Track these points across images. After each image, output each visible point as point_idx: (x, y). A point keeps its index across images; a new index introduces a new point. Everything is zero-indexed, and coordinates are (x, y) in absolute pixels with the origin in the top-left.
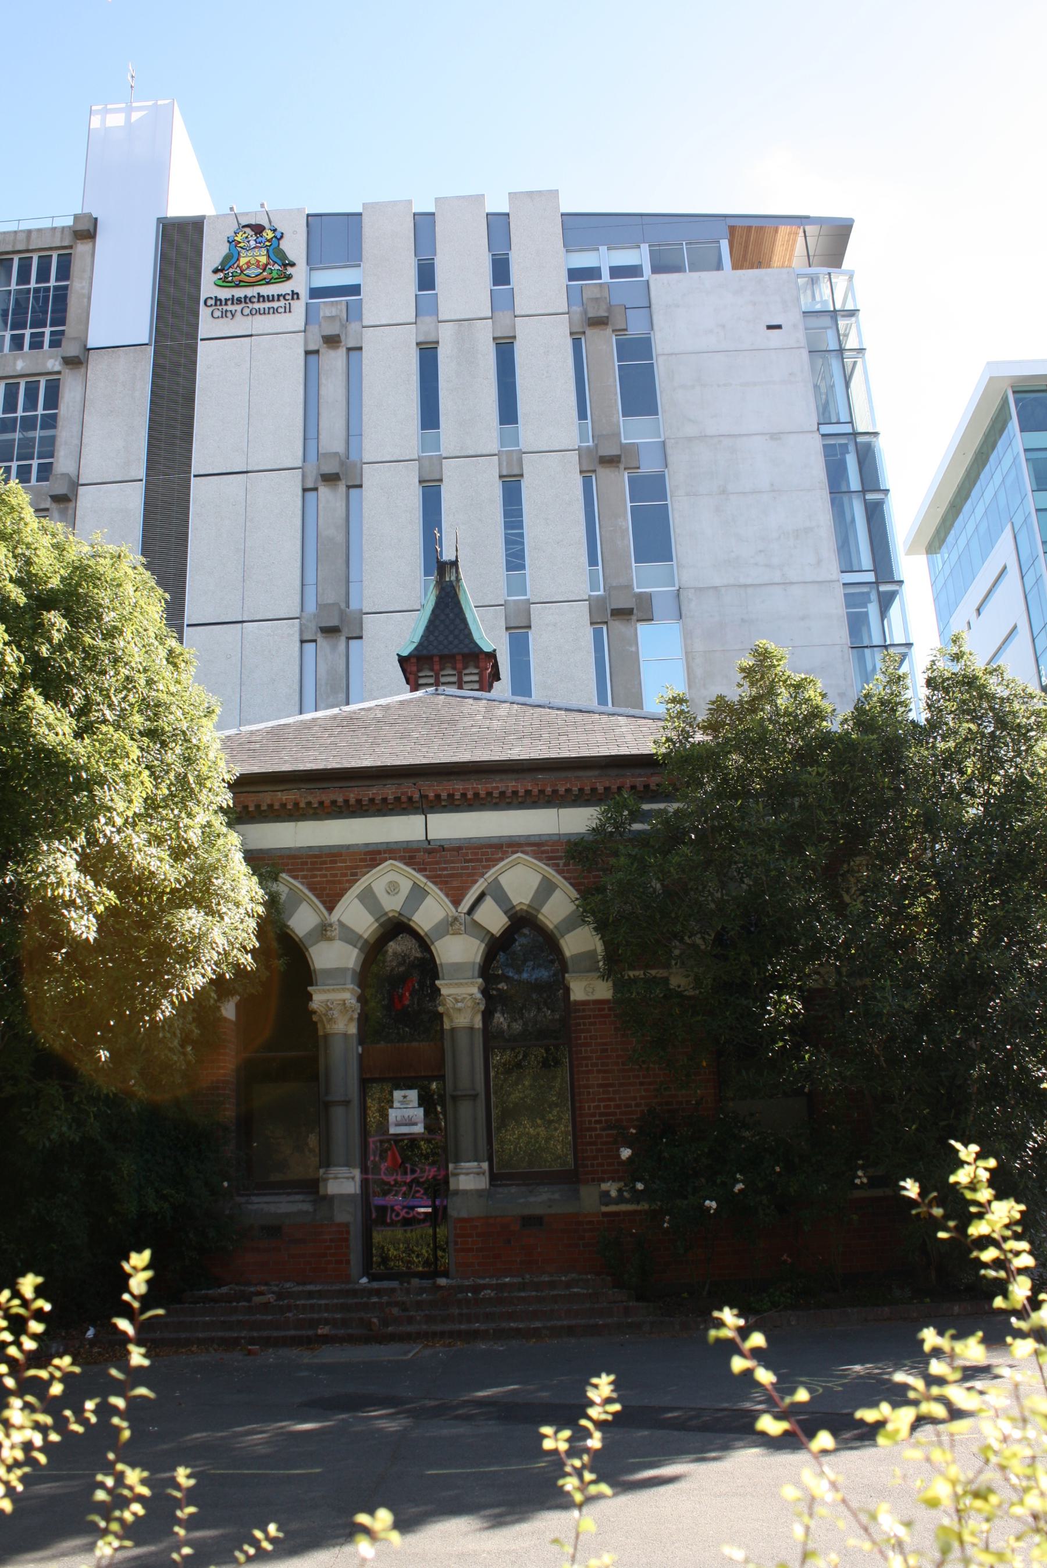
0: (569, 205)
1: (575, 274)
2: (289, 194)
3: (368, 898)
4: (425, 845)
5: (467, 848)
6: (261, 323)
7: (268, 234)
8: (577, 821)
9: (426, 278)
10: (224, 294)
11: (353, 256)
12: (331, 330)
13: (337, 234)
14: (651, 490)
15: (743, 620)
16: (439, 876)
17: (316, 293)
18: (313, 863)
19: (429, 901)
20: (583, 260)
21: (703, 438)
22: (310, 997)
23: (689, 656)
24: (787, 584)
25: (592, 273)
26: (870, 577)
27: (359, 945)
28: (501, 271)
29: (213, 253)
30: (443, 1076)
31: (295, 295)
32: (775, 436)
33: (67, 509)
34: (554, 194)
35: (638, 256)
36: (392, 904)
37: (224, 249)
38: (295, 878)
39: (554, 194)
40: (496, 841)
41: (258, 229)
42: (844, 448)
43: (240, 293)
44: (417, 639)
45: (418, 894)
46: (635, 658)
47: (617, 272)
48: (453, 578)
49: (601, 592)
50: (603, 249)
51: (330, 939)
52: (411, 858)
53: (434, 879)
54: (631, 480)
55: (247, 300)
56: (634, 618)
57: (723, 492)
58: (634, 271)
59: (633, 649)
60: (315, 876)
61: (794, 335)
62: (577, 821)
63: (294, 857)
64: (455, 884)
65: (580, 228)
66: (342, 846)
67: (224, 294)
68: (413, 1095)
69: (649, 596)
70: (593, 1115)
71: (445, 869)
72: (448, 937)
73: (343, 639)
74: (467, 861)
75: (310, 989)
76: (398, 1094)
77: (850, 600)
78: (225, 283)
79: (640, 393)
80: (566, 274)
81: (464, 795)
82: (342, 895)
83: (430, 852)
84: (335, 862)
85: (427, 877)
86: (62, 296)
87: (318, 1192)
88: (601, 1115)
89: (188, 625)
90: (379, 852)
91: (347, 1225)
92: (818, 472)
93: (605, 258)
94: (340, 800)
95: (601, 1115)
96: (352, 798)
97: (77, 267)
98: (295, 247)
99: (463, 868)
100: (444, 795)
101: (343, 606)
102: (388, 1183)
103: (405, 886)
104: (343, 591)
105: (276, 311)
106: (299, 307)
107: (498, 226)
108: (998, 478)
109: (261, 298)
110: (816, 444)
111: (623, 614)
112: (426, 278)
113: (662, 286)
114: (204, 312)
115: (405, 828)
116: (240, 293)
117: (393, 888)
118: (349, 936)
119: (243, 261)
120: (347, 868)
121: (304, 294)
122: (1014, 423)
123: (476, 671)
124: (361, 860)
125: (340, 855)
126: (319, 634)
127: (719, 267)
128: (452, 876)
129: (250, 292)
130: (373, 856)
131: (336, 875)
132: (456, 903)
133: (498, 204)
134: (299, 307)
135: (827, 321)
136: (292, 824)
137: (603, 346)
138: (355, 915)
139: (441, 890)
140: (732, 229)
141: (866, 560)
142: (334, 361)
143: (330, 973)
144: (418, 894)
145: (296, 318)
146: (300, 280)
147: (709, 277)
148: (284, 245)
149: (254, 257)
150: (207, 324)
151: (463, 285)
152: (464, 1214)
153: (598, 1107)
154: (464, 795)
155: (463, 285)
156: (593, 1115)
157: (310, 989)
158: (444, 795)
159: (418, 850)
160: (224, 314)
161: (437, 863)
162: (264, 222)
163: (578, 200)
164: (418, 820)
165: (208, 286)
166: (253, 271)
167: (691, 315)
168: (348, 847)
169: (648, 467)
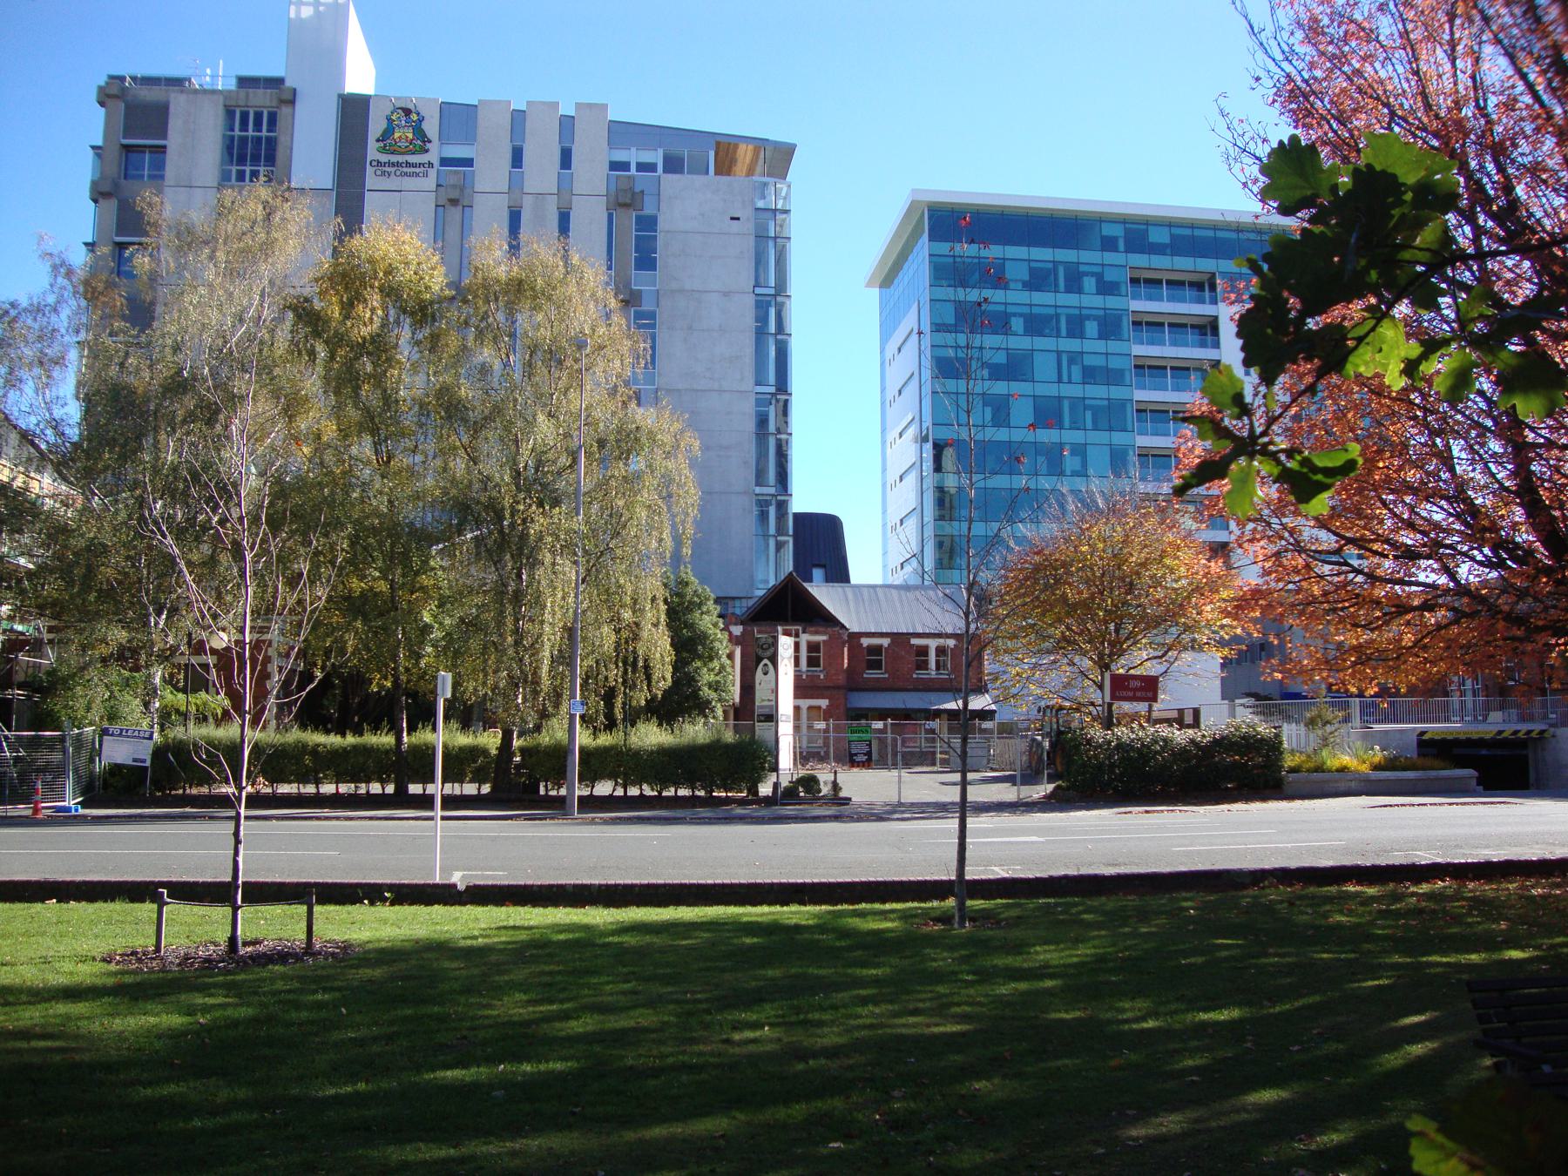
0: (613, 115)
1: (616, 166)
2: (432, 86)
6: (409, 183)
7: (414, 117)
9: (517, 158)
10: (384, 158)
11: (470, 137)
12: (454, 195)
13: (460, 118)
14: (648, 224)
17: (445, 162)
20: (620, 156)
21: (681, 291)
24: (721, 391)
25: (624, 166)
26: (773, 390)
28: (566, 159)
29: (376, 127)
31: (431, 165)
32: (726, 294)
34: (604, 107)
35: (657, 157)
37: (384, 125)
39: (604, 107)
41: (407, 112)
42: (768, 304)
43: (394, 158)
47: (642, 167)
50: (633, 150)
54: (638, 217)
55: (398, 164)
57: (690, 328)
58: (651, 167)
61: (747, 226)
65: (622, 132)
67: (384, 158)
69: (640, 292)
77: (759, 403)
78: (383, 150)
79: (646, 261)
80: (607, 166)
86: (272, 143)
92: (749, 321)
93: (633, 156)
97: (281, 123)
98: (431, 128)
105: (418, 175)
106: (433, 173)
107: (567, 124)
108: (911, 272)
109: (408, 164)
110: (750, 301)
112: (517, 158)
113: (670, 182)
114: (369, 170)
116: (394, 158)
119: (397, 135)
121: (436, 162)
122: (926, 236)
127: (707, 173)
129: (400, 158)
133: (567, 109)
134: (433, 173)
135: (770, 214)
137: (629, 219)
140: (718, 144)
141: (772, 378)
142: (455, 213)
145: (430, 182)
146: (433, 156)
147: (699, 180)
148: (425, 126)
149: (404, 134)
150: (372, 179)
151: (541, 173)
155: (541, 173)
160: (383, 173)
162: (411, 107)
163: (618, 112)
165: (373, 152)
166: (403, 144)
167: (685, 204)
169: (647, 307)
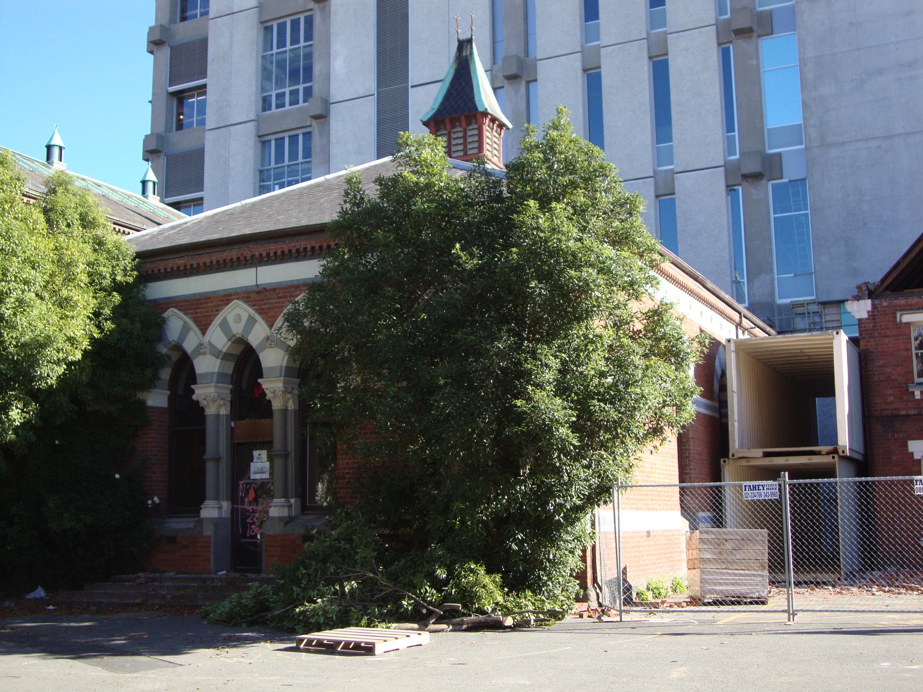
3: (224, 325)
4: (256, 289)
5: (280, 289)
8: (308, 270)
15: (851, 24)
16: (263, 309)
18: (196, 304)
19: (257, 326)
22: (193, 392)
23: (802, 63)
27: (221, 357)
30: (271, 443)
33: (325, 7)
36: (237, 329)
38: (186, 314)
40: (296, 283)
44: (436, 107)
45: (251, 322)
46: (757, 70)
48: (468, 53)
49: (728, 16)
51: (204, 354)
52: (248, 297)
53: (260, 311)
56: (755, 35)
59: (754, 62)
60: (197, 313)
62: (308, 270)
63: (187, 301)
64: (272, 313)
66: (211, 292)
68: (264, 453)
70: (345, 469)
71: (266, 304)
72: (267, 350)
73: (523, 83)
74: (279, 298)
75: (259, 380)
76: (256, 453)
81: (276, 253)
82: (209, 325)
83: (258, 293)
84: (207, 303)
85: (256, 310)
87: (199, 516)
88: (349, 468)
89: (412, 87)
90: (230, 295)
91: (209, 537)
94: (208, 261)
95: (349, 468)
96: (214, 259)
99: (276, 303)
100: (264, 254)
101: (523, 56)
102: (248, 511)
103: (245, 317)
104: (522, 44)
111: (743, 33)
115: (244, 278)
117: (238, 318)
118: (216, 353)
120: (214, 306)
123: (476, 126)
124: (222, 301)
125: (209, 298)
126: (506, 81)
128: (269, 308)
130: (226, 298)
131: (207, 312)
132: (271, 326)
136: (185, 279)
138: (217, 337)
139: (263, 318)
143: (204, 375)
144: (251, 322)
152: (271, 533)
153: (348, 463)
154: (276, 253)
156: (345, 469)
157: (259, 380)
158: (264, 254)
159: (251, 292)
161: (262, 300)
164: (251, 271)
168: (215, 292)
